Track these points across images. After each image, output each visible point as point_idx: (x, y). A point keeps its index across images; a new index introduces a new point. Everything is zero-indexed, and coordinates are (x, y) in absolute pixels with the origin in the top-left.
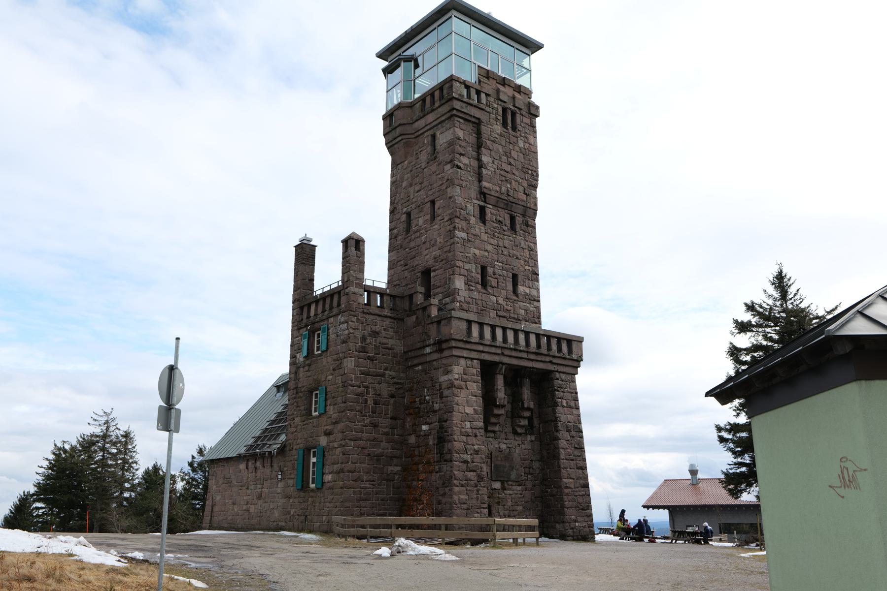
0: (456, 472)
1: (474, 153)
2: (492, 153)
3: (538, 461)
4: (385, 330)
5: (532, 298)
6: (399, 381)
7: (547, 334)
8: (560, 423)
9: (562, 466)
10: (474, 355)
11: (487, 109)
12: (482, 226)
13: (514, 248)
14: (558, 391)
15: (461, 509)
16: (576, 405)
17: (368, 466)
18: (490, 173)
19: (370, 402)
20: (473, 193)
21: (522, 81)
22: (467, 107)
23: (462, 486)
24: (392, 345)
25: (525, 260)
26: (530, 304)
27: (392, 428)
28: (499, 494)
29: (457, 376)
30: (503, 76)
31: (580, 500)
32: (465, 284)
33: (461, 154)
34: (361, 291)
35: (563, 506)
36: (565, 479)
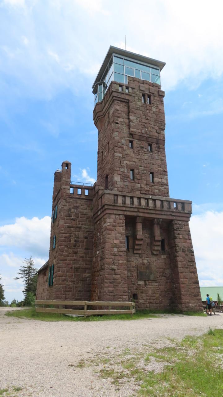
0: (106, 275)
1: (126, 116)
2: (136, 115)
3: (169, 269)
4: (82, 205)
5: (163, 184)
6: (90, 230)
7: (175, 201)
8: (178, 247)
9: (180, 271)
10: (120, 212)
11: (133, 95)
12: (131, 150)
13: (152, 160)
14: (176, 230)
15: (109, 296)
16: (189, 238)
17: (71, 274)
18: (135, 124)
19: (73, 241)
20: (126, 134)
21: (158, 82)
22: (121, 95)
23: (110, 283)
24: (86, 213)
25: (158, 165)
26: (162, 187)
27: (86, 254)
28: (143, 287)
29: (109, 224)
30: (143, 79)
31: (193, 291)
32: (121, 178)
33: (118, 117)
34: (68, 187)
35: (181, 294)
36: (182, 278)
